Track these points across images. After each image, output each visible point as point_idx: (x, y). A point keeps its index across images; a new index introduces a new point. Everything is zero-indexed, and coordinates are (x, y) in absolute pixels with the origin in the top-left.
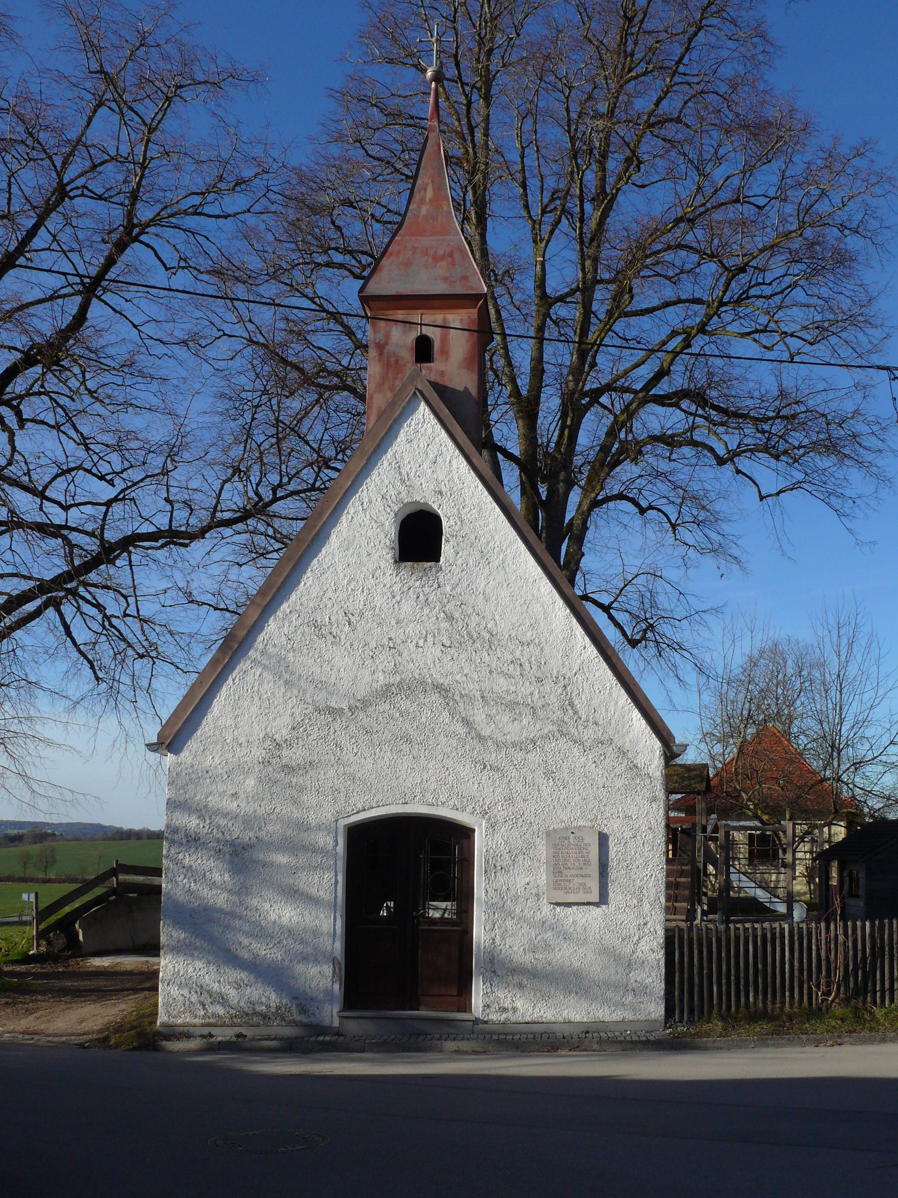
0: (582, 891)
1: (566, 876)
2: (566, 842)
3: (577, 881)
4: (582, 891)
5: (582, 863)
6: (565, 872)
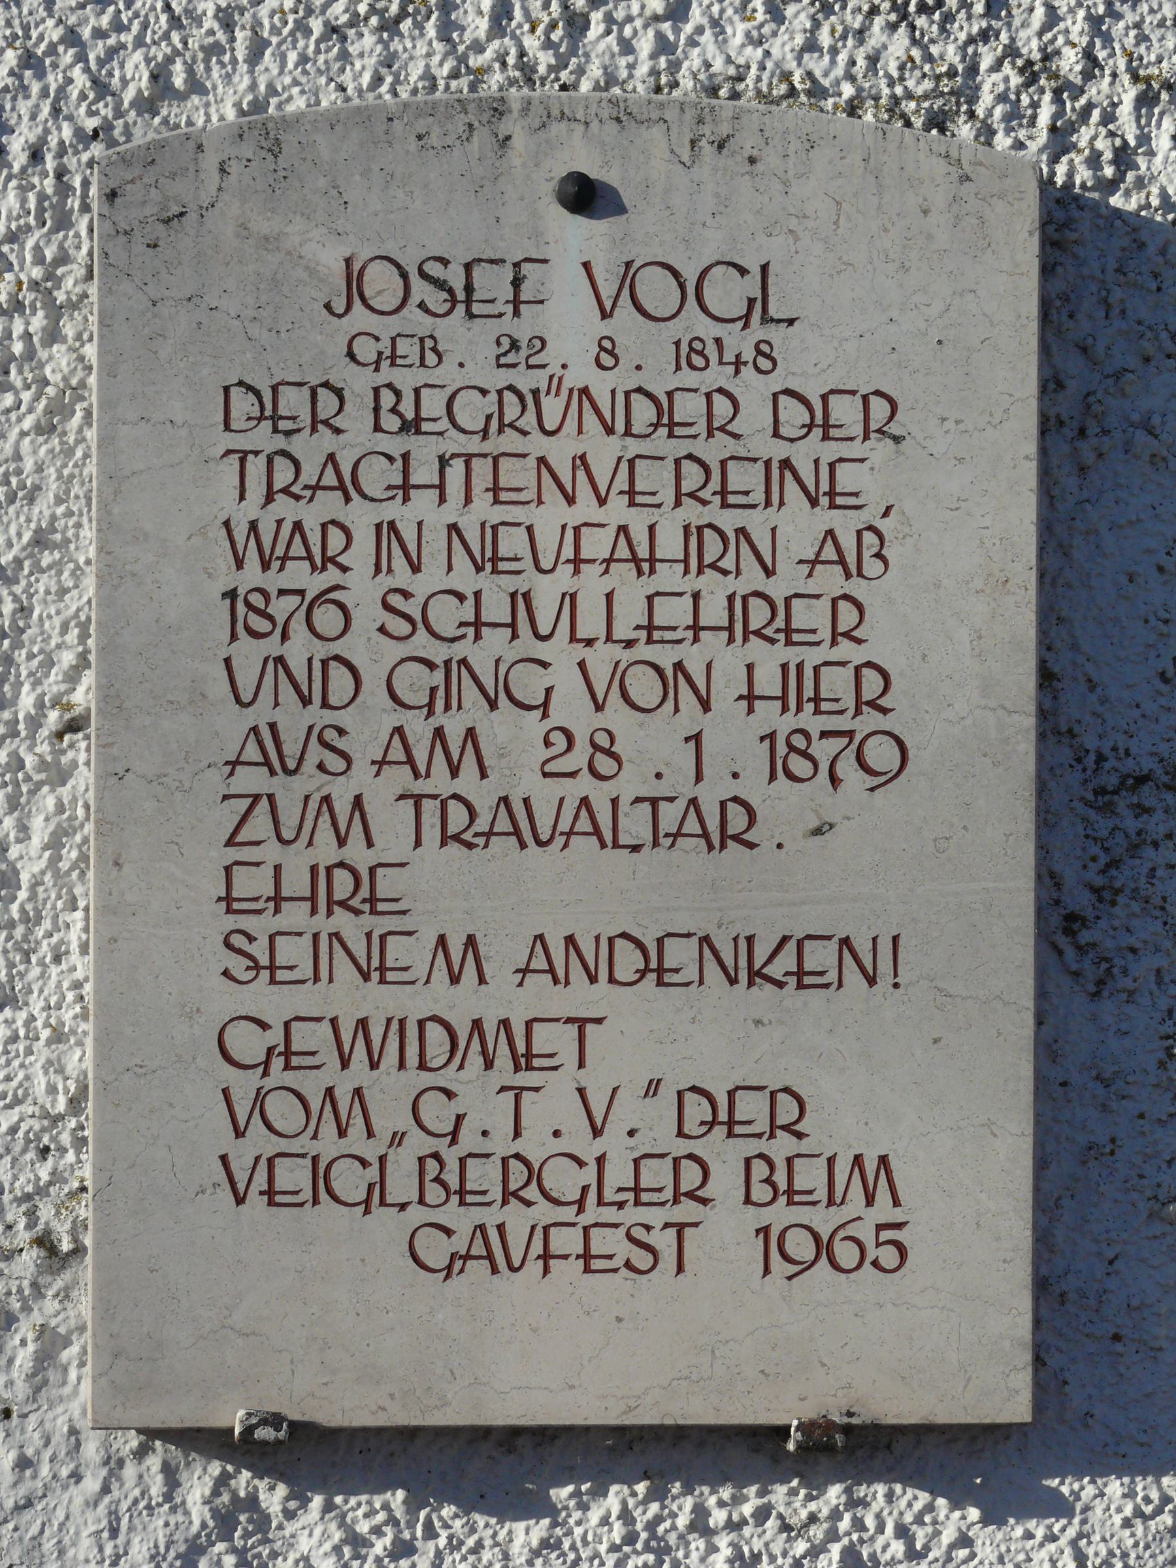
0: (727, 1229)
1: (462, 958)
2: (469, 347)
3: (656, 1042)
4: (727, 1229)
5: (735, 737)
6: (439, 888)
